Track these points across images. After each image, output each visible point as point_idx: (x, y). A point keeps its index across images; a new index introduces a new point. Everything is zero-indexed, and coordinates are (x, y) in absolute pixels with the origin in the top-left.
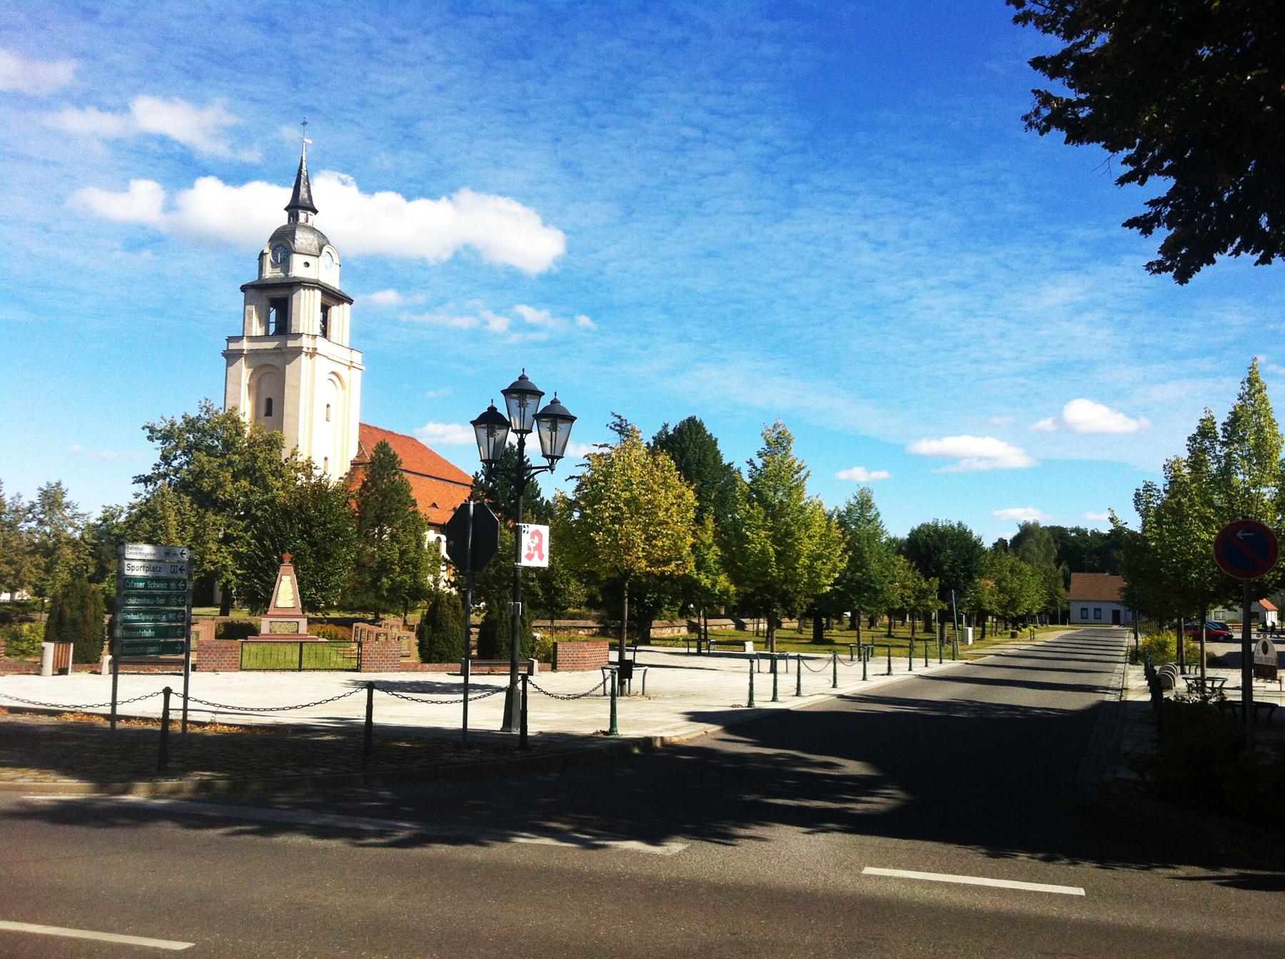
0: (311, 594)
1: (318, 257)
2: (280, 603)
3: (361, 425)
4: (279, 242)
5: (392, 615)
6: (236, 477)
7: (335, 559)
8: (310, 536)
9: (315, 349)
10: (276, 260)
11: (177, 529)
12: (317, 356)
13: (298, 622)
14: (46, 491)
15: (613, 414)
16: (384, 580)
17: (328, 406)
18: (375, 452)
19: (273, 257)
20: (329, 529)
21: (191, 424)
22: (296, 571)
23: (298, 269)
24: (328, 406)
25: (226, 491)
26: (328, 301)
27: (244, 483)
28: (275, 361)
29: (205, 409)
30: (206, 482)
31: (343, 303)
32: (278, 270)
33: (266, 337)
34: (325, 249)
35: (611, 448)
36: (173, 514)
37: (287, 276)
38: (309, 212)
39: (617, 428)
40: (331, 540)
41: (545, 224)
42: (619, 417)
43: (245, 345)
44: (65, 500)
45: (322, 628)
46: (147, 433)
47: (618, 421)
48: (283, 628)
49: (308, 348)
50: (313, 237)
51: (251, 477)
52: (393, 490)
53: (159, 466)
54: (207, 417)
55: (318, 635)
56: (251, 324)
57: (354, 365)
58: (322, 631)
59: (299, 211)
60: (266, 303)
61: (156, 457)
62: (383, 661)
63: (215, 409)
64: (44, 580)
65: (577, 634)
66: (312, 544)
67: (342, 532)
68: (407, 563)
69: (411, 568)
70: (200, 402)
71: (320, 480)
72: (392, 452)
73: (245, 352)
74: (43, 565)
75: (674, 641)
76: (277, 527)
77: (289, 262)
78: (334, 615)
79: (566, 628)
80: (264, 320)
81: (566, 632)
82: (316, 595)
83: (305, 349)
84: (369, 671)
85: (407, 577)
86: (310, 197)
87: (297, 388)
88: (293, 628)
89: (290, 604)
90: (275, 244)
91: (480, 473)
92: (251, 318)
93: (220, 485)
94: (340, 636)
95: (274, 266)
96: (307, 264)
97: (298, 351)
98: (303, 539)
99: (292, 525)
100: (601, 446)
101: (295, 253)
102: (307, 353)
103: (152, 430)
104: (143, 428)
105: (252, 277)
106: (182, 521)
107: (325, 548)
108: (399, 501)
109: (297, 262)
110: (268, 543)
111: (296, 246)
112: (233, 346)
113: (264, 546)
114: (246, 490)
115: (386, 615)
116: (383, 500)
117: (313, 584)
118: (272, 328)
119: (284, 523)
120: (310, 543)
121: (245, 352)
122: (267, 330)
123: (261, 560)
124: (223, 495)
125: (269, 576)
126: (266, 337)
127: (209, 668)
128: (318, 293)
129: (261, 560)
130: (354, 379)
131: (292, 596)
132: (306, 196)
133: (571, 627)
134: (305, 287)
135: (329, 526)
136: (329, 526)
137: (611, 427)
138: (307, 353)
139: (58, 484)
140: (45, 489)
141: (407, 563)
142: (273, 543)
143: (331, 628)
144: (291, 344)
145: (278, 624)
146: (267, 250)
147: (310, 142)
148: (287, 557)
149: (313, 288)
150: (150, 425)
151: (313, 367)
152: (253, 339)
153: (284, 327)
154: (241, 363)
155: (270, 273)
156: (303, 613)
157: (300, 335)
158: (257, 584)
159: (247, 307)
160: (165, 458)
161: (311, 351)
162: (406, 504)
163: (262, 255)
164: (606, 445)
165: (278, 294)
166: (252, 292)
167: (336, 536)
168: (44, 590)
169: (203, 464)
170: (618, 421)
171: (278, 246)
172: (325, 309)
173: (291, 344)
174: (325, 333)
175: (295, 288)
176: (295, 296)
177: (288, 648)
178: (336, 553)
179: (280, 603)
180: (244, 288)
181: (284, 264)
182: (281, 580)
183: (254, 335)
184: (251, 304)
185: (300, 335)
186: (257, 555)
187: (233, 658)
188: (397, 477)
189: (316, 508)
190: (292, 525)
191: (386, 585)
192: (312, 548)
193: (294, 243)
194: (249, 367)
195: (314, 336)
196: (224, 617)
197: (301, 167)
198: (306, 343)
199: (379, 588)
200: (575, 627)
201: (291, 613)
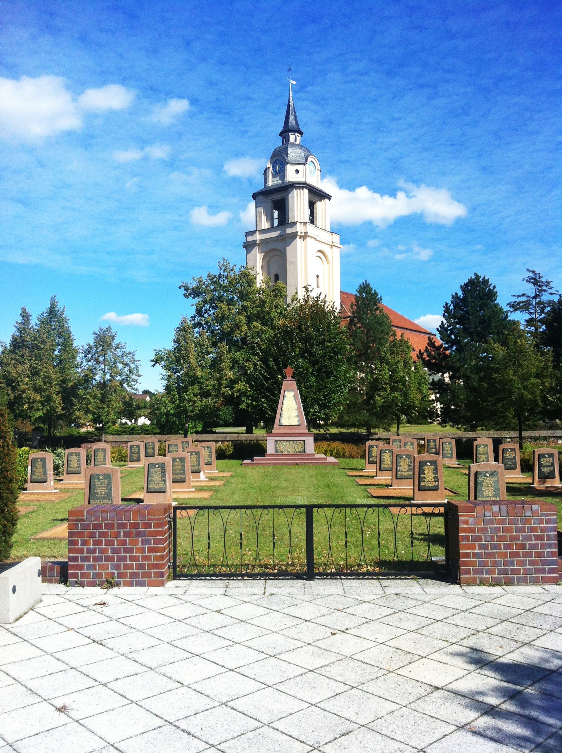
0: (315, 412)
1: (305, 164)
2: (285, 421)
3: (341, 292)
4: (277, 158)
5: (382, 430)
6: (249, 320)
7: (336, 376)
8: (311, 354)
9: (306, 233)
10: (275, 172)
11: (197, 359)
12: (308, 239)
13: (304, 441)
14: (99, 335)
15: (528, 270)
16: (377, 398)
17: (318, 276)
18: (359, 292)
20: (328, 347)
21: (215, 280)
22: (299, 388)
23: (291, 176)
24: (318, 276)
25: (242, 331)
26: (314, 198)
27: (257, 325)
28: (278, 246)
29: (224, 268)
30: (227, 325)
31: (324, 199)
32: (278, 178)
33: (272, 229)
34: (310, 159)
35: (528, 297)
36: (193, 345)
37: (283, 182)
38: (297, 134)
39: (532, 281)
40: (331, 358)
42: (533, 272)
43: (258, 237)
44: (116, 341)
45: (329, 445)
46: (183, 291)
47: (532, 275)
48: (289, 448)
49: (301, 233)
51: (262, 320)
52: (376, 322)
53: (195, 317)
54: (226, 274)
55: (326, 453)
56: (261, 221)
57: (334, 244)
58: (329, 448)
60: (270, 205)
61: (192, 311)
62: (516, 555)
63: (231, 267)
64: (100, 408)
65: (556, 443)
66: (314, 363)
67: (341, 349)
68: (397, 382)
69: (401, 387)
70: (219, 262)
71: (317, 301)
72: (373, 291)
74: (99, 395)
76: (280, 349)
78: (334, 430)
79: (545, 438)
81: (545, 442)
82: (319, 412)
83: (299, 234)
84: (482, 583)
85: (398, 395)
86: (297, 123)
87: (295, 264)
88: (300, 446)
89: (295, 422)
90: (274, 159)
91: (450, 303)
92: (260, 217)
93: (238, 327)
94: (347, 454)
95: (274, 176)
96: (297, 171)
97: (294, 236)
98: (305, 358)
99: (293, 345)
100: (519, 296)
101: (288, 163)
102: (301, 237)
103: (186, 289)
104: (180, 288)
105: (261, 187)
106: (201, 352)
107: (326, 366)
108: (382, 332)
109: (290, 169)
110: (271, 363)
111: (289, 159)
112: (250, 239)
113: (268, 366)
114: (257, 330)
115: (377, 430)
116: (368, 332)
117: (316, 401)
118: (276, 223)
119: (286, 343)
120: (311, 362)
123: (267, 380)
124: (240, 334)
125: (273, 394)
126: (272, 229)
127: (98, 575)
128: (306, 191)
129: (267, 380)
130: (335, 255)
131: (296, 413)
133: (550, 437)
134: (297, 188)
135: (328, 344)
136: (328, 344)
137: (527, 281)
138: (301, 237)
139: (109, 329)
140: (99, 333)
141: (397, 382)
142: (277, 364)
143: (337, 445)
144: (289, 231)
145: (284, 443)
146: (269, 165)
148: (289, 371)
149: (303, 188)
150: (184, 285)
151: (306, 247)
152: (263, 231)
153: (284, 221)
154: (256, 250)
155: (272, 182)
156: (309, 429)
157: (295, 223)
158: (264, 403)
159: (258, 209)
160: (199, 312)
161: (303, 234)
162: (388, 333)
163: (267, 169)
164: (523, 295)
165: (278, 197)
166: (260, 198)
167: (336, 354)
168: (101, 416)
169: (224, 311)
170: (532, 275)
171: (276, 161)
172: (312, 205)
173: (289, 231)
174: (312, 221)
175: (289, 190)
176: (290, 196)
177: (281, 518)
178: (336, 370)
179: (285, 421)
180: (255, 197)
181: (280, 172)
182: (284, 396)
183: (263, 228)
184: (260, 207)
185: (295, 223)
186: (263, 375)
187: (151, 550)
188: (378, 312)
189: (314, 326)
190: (293, 345)
191: (379, 402)
192: (313, 366)
193: (287, 157)
194: (261, 252)
195: (305, 223)
196: (249, 435)
197: (289, 102)
198: (299, 229)
199: (374, 406)
200: (554, 437)
201: (296, 431)
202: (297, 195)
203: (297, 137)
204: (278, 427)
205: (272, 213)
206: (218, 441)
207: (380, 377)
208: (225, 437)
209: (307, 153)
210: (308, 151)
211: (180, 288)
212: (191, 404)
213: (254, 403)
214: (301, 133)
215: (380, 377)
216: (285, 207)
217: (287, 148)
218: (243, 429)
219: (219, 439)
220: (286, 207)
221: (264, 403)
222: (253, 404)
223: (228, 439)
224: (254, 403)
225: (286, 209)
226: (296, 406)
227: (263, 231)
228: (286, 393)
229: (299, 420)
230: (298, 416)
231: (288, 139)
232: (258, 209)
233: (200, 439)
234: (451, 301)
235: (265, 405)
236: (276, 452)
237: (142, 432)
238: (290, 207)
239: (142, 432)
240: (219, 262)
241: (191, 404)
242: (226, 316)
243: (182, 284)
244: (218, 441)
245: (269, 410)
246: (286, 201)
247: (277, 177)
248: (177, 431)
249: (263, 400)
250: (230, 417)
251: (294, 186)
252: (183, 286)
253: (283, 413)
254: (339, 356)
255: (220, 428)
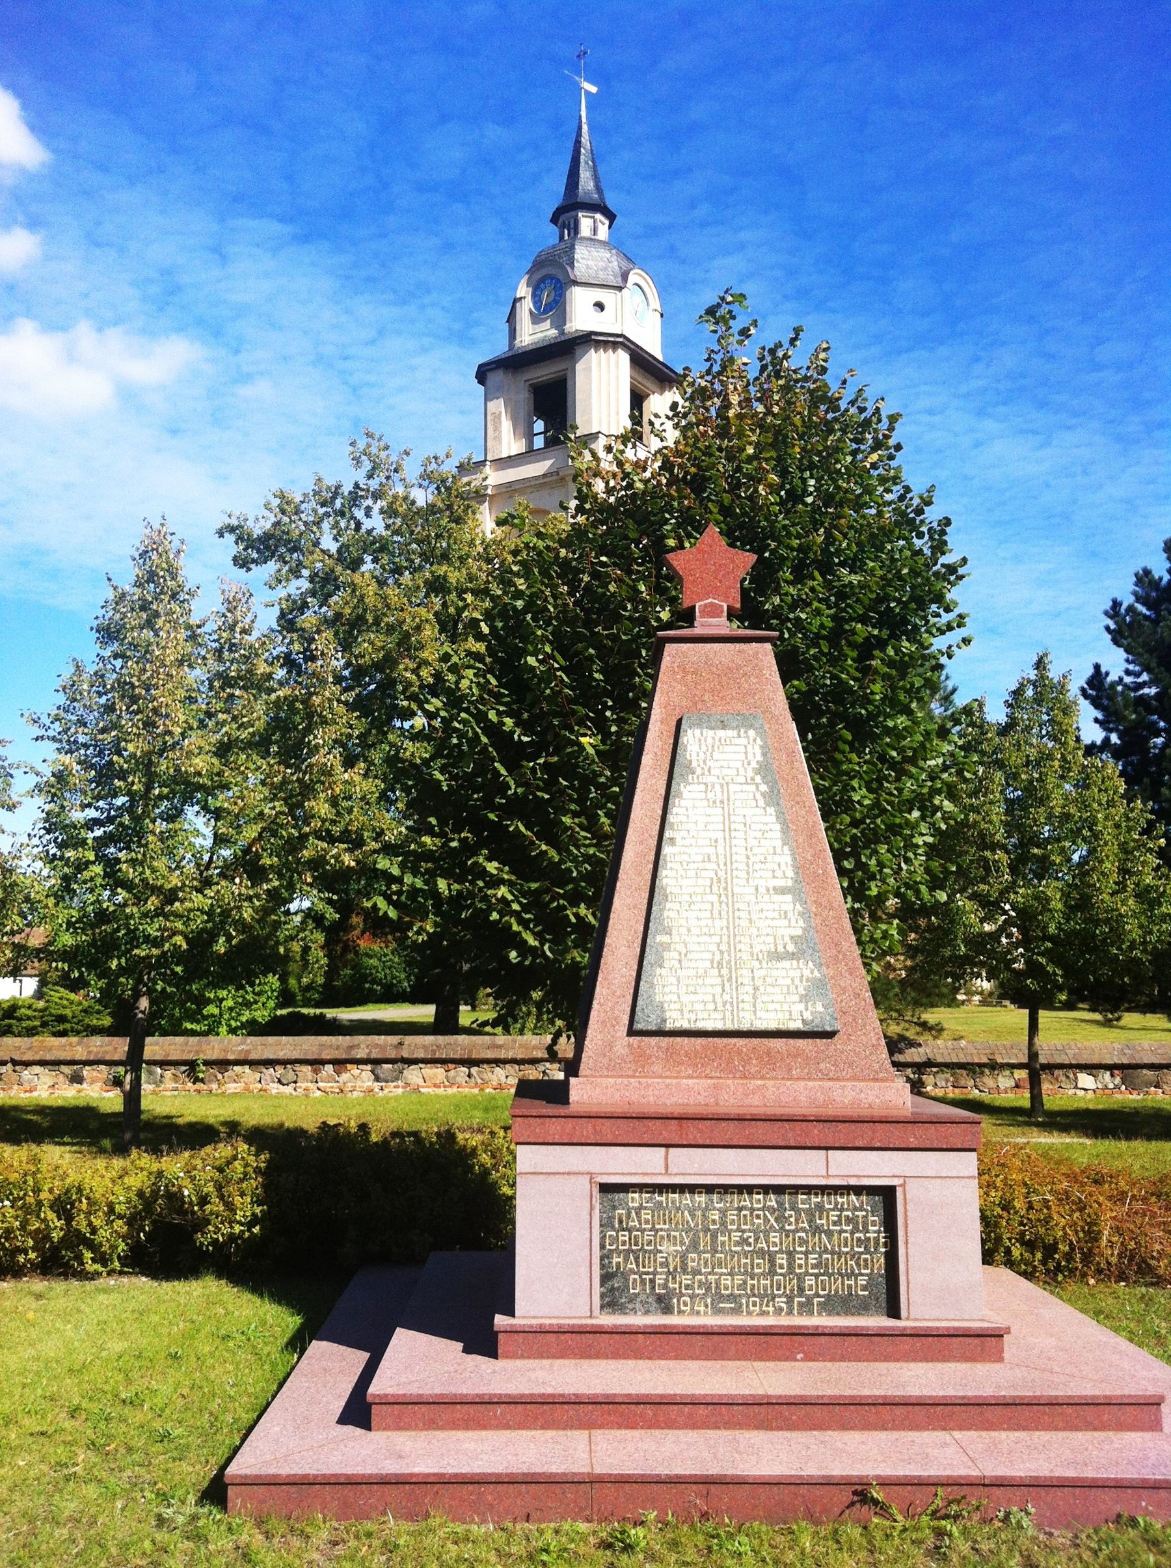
1: (620, 289)
4: (544, 272)
10: (538, 309)
13: (886, 1196)
19: (535, 303)
26: (647, 383)
31: (671, 389)
32: (547, 325)
33: (530, 454)
34: (633, 278)
37: (562, 333)
38: (598, 216)
41: (448, 1136)
50: (608, 255)
54: (374, 484)
59: (580, 214)
60: (524, 396)
63: (394, 458)
70: (353, 444)
73: (489, 491)
75: (1084, 1009)
77: (564, 304)
80: (521, 430)
90: (537, 276)
92: (497, 428)
93: (406, 644)
94: (1108, 1249)
95: (536, 319)
96: (600, 306)
101: (575, 283)
104: (221, 535)
105: (498, 348)
118: (539, 442)
121: (489, 491)
122: (530, 443)
123: (513, 754)
124: (415, 671)
129: (513, 754)
132: (591, 185)
147: (593, 89)
149: (615, 345)
150: (235, 523)
152: (504, 463)
155: (530, 334)
165: (544, 373)
166: (496, 377)
171: (542, 280)
175: (578, 351)
176: (579, 367)
183: (504, 455)
186: (494, 730)
193: (573, 267)
197: (579, 134)
202: (600, 364)
203: (600, 225)
204: (622, 1042)
205: (531, 425)
206: (323, 1062)
207: (972, 817)
208: (351, 1048)
209: (625, 264)
210: (629, 259)
211: (221, 535)
212: (153, 903)
213: (442, 884)
214: (611, 216)
215: (972, 817)
216: (565, 401)
217: (573, 245)
218: (426, 1013)
219: (326, 1055)
220: (569, 399)
221: (496, 882)
222: (435, 894)
223: (361, 1054)
224: (442, 884)
225: (569, 403)
226: (786, 858)
227: (504, 463)
228: (690, 738)
229: (817, 988)
230: (801, 950)
231: (576, 229)
232: (491, 405)
233: (254, 1056)
234: (1135, 594)
235: (503, 891)
236: (612, 1301)
237: (44, 1024)
238: (578, 397)
239: (44, 1024)
240: (353, 444)
241: (153, 903)
242: (370, 618)
243: (227, 521)
244: (323, 1062)
245: (524, 923)
246: (569, 383)
247: (545, 320)
248: (179, 1021)
249: (492, 867)
250: (403, 976)
251: (589, 340)
252: (232, 529)
253: (669, 912)
254: (905, 644)
255: (371, 1006)
